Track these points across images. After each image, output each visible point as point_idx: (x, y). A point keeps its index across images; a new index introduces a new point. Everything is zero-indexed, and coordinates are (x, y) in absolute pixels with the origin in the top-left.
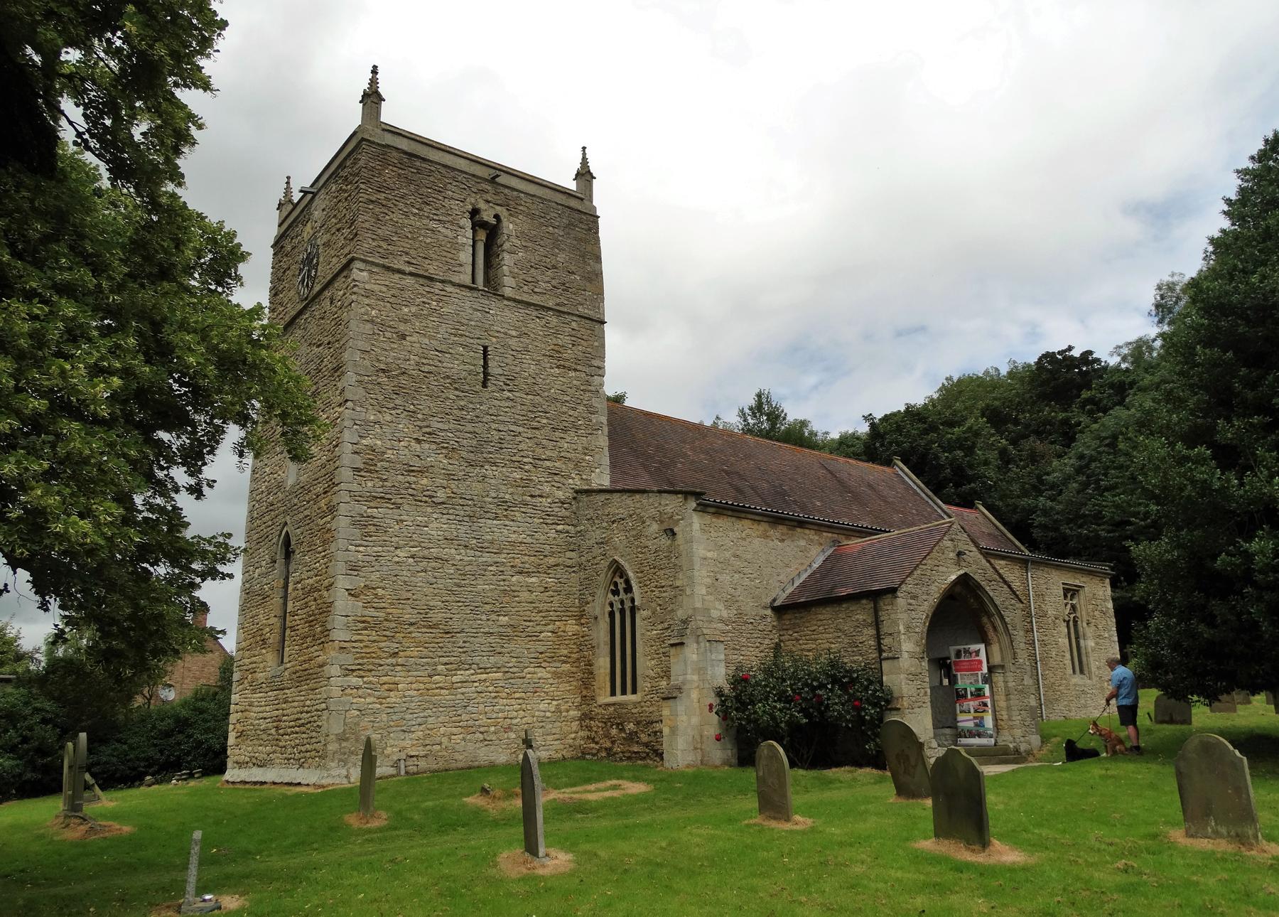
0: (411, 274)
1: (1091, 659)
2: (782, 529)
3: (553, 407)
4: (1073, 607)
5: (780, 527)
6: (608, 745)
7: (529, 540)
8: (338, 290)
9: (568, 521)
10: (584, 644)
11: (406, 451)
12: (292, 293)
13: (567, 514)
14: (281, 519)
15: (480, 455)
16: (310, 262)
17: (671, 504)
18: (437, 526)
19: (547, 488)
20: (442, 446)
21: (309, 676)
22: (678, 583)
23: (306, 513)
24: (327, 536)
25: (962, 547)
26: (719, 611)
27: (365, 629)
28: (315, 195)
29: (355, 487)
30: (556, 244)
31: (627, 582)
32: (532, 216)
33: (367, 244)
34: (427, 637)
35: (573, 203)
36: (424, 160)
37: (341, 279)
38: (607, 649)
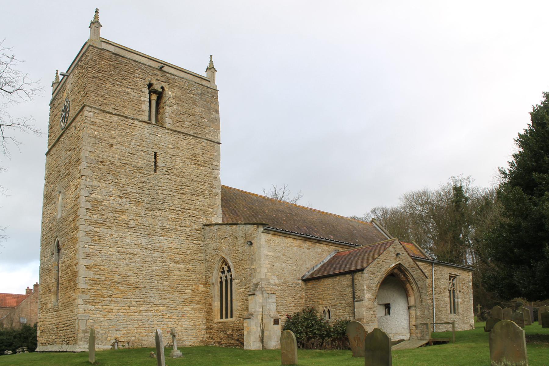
0: (116, 115)
1: (460, 307)
2: (308, 244)
3: (192, 184)
4: (453, 284)
5: (308, 242)
6: (219, 340)
7: (179, 247)
8: (78, 122)
9: (199, 239)
10: (208, 297)
11: (114, 202)
12: (58, 126)
13: (199, 235)
14: (55, 235)
15: (152, 205)
16: (66, 110)
17: (250, 228)
18: (130, 238)
19: (188, 223)
20: (132, 200)
21: (69, 304)
22: (253, 267)
23: (66, 230)
24: (75, 240)
25: (399, 252)
26: (274, 280)
27: (95, 284)
28: (68, 76)
29: (87, 217)
30: (195, 103)
31: (229, 267)
32: (181, 88)
33: (92, 98)
34: (127, 289)
35: (204, 83)
36: (123, 57)
37: (79, 116)
38: (219, 298)
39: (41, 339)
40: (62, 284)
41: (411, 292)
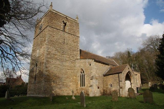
11: (53, 52)
15: (63, 53)
17: (90, 60)
18: (58, 62)
19: (72, 58)
20: (58, 52)
38: (80, 80)
39: (29, 92)
40: (37, 76)
41: (132, 79)
